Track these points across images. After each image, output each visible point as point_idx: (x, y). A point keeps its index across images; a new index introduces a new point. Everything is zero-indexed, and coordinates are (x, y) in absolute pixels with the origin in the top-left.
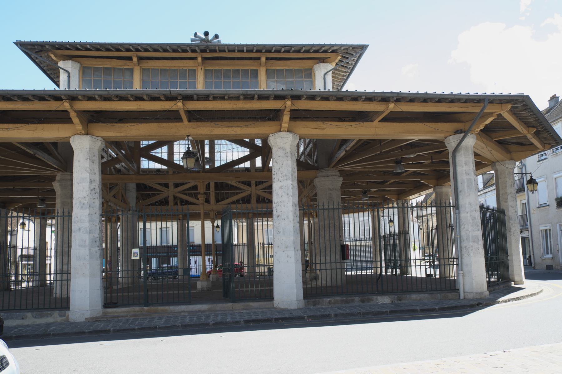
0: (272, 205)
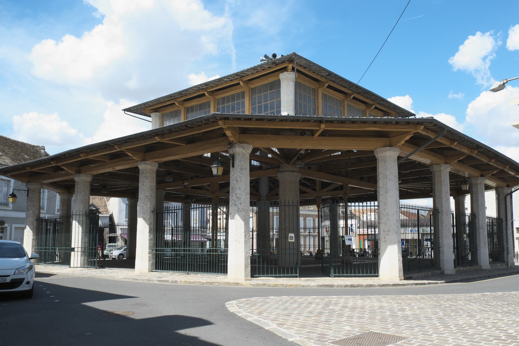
0: (377, 185)
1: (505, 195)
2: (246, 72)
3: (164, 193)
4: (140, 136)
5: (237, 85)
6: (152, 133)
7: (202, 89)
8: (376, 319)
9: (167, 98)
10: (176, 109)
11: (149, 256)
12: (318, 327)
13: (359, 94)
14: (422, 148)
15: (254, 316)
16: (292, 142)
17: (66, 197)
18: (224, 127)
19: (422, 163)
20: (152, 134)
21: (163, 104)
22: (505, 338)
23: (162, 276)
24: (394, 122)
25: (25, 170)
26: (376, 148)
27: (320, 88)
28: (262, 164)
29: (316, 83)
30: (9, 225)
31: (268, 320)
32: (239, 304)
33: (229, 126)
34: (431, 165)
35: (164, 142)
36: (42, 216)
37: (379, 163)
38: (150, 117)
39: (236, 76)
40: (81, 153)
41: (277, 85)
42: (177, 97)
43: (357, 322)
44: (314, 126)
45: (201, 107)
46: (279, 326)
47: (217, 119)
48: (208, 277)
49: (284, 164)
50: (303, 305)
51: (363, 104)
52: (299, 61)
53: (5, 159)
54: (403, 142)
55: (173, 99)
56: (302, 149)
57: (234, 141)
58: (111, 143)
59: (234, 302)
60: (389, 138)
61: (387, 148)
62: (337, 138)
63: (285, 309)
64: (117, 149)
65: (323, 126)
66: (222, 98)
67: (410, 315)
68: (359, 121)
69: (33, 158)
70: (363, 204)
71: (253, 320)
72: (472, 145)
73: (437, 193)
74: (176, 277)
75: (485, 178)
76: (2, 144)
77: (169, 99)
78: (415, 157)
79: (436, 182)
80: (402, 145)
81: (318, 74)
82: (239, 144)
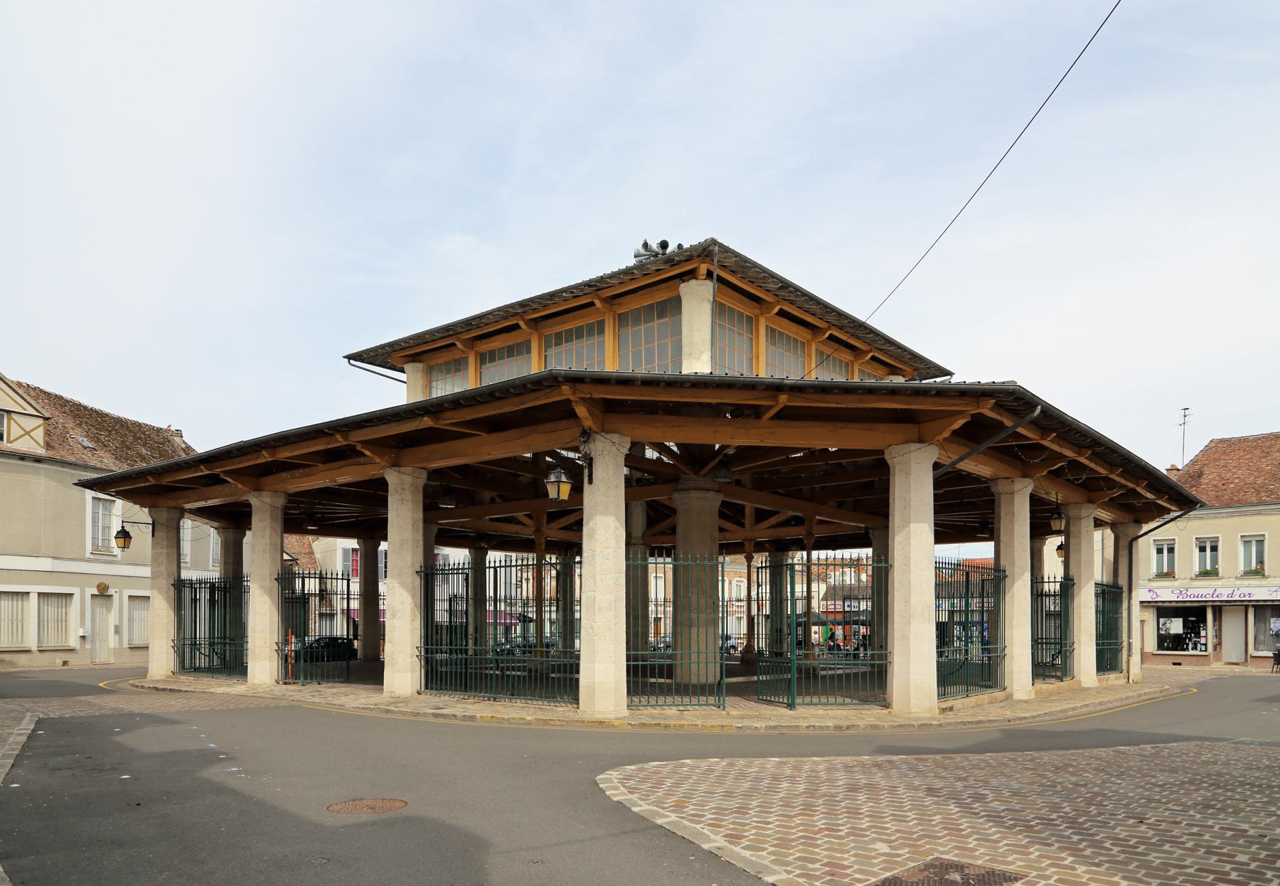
1: (1130, 539)
2: (608, 280)
3: (435, 529)
4: (390, 416)
5: (578, 310)
6: (418, 409)
7: (515, 315)
8: (934, 823)
9: (438, 332)
10: (456, 356)
11: (412, 662)
12: (817, 846)
13: (841, 329)
14: (983, 447)
15: (667, 813)
16: (715, 432)
17: (231, 534)
18: (572, 398)
19: (974, 474)
20: (417, 412)
21: (430, 346)
22: (1237, 876)
23: (441, 705)
24: (934, 392)
25: (146, 482)
26: (890, 445)
27: (762, 314)
28: (633, 471)
29: (754, 304)
30: (116, 592)
31: (702, 825)
32: (625, 781)
33: (583, 396)
34: (994, 480)
35: (442, 427)
36: (185, 575)
37: (894, 476)
38: (404, 372)
39: (587, 287)
40: (264, 448)
41: (673, 306)
42: (460, 330)
43: (897, 831)
44: (765, 398)
45: (511, 351)
46: (731, 843)
47: (558, 381)
48: (538, 706)
50: (762, 783)
51: (849, 351)
52: (722, 256)
53: (101, 457)
54: (946, 434)
55: (451, 336)
56: (730, 446)
57: (594, 428)
58: (328, 429)
59: (614, 775)
60: (917, 425)
61: (914, 446)
62: (809, 423)
63: (729, 794)
64: (340, 441)
65: (783, 399)
66: (556, 334)
67: (1003, 810)
68: (860, 390)
69: (159, 454)
71: (667, 823)
72: (1083, 439)
73: (1003, 537)
74: (470, 706)
75: (1096, 506)
76: (94, 426)
77: (442, 335)
78: (969, 466)
79: (1002, 515)
80: (945, 439)
81: (760, 287)
82: (603, 434)
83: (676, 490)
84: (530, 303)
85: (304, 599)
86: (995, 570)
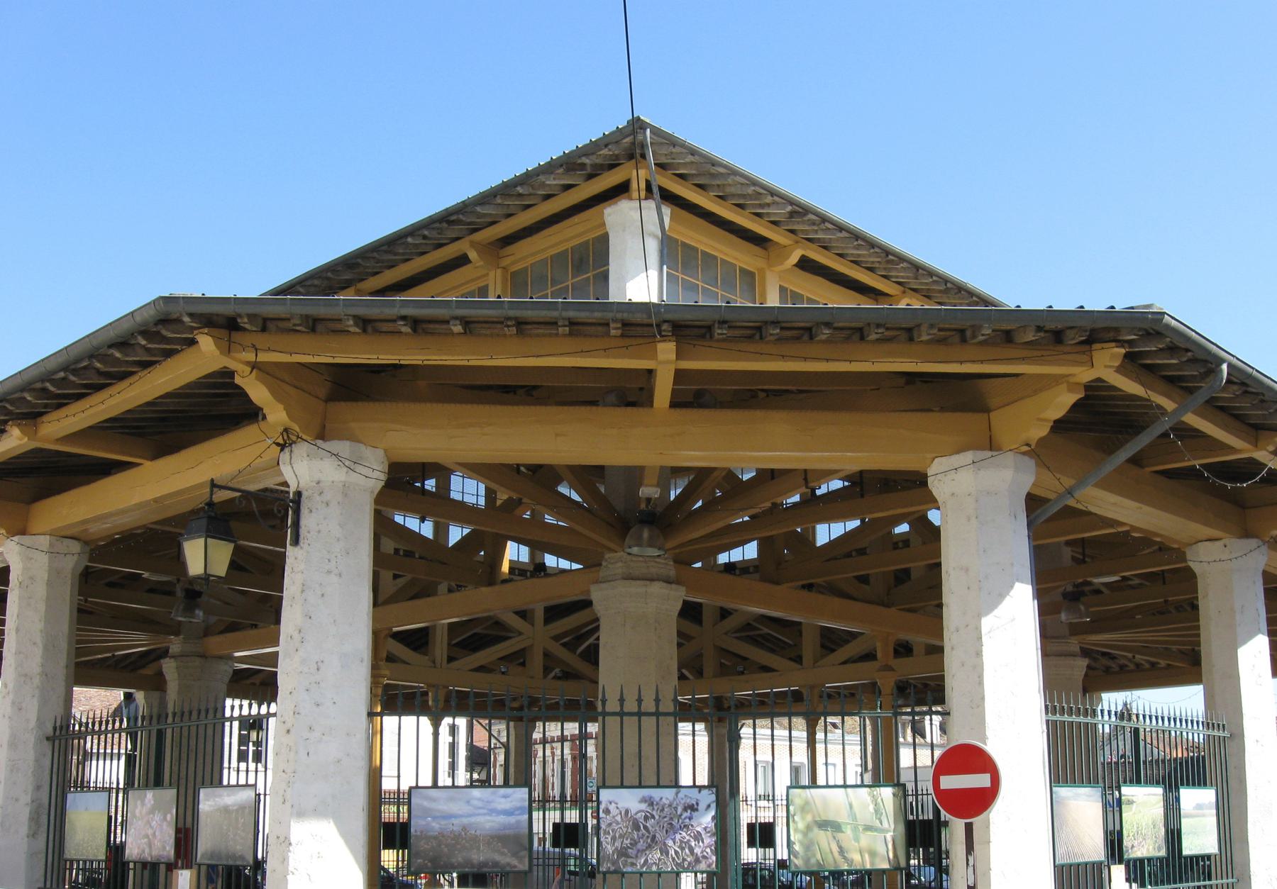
16: (557, 435)
39: (445, 225)
49: (616, 552)
70: (454, 722)
83: (597, 582)
84: (359, 261)
85: (259, 795)
86: (1207, 725)
